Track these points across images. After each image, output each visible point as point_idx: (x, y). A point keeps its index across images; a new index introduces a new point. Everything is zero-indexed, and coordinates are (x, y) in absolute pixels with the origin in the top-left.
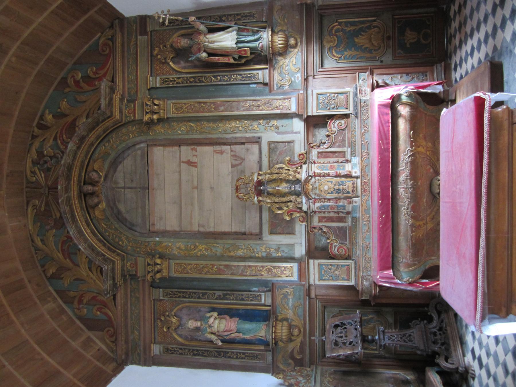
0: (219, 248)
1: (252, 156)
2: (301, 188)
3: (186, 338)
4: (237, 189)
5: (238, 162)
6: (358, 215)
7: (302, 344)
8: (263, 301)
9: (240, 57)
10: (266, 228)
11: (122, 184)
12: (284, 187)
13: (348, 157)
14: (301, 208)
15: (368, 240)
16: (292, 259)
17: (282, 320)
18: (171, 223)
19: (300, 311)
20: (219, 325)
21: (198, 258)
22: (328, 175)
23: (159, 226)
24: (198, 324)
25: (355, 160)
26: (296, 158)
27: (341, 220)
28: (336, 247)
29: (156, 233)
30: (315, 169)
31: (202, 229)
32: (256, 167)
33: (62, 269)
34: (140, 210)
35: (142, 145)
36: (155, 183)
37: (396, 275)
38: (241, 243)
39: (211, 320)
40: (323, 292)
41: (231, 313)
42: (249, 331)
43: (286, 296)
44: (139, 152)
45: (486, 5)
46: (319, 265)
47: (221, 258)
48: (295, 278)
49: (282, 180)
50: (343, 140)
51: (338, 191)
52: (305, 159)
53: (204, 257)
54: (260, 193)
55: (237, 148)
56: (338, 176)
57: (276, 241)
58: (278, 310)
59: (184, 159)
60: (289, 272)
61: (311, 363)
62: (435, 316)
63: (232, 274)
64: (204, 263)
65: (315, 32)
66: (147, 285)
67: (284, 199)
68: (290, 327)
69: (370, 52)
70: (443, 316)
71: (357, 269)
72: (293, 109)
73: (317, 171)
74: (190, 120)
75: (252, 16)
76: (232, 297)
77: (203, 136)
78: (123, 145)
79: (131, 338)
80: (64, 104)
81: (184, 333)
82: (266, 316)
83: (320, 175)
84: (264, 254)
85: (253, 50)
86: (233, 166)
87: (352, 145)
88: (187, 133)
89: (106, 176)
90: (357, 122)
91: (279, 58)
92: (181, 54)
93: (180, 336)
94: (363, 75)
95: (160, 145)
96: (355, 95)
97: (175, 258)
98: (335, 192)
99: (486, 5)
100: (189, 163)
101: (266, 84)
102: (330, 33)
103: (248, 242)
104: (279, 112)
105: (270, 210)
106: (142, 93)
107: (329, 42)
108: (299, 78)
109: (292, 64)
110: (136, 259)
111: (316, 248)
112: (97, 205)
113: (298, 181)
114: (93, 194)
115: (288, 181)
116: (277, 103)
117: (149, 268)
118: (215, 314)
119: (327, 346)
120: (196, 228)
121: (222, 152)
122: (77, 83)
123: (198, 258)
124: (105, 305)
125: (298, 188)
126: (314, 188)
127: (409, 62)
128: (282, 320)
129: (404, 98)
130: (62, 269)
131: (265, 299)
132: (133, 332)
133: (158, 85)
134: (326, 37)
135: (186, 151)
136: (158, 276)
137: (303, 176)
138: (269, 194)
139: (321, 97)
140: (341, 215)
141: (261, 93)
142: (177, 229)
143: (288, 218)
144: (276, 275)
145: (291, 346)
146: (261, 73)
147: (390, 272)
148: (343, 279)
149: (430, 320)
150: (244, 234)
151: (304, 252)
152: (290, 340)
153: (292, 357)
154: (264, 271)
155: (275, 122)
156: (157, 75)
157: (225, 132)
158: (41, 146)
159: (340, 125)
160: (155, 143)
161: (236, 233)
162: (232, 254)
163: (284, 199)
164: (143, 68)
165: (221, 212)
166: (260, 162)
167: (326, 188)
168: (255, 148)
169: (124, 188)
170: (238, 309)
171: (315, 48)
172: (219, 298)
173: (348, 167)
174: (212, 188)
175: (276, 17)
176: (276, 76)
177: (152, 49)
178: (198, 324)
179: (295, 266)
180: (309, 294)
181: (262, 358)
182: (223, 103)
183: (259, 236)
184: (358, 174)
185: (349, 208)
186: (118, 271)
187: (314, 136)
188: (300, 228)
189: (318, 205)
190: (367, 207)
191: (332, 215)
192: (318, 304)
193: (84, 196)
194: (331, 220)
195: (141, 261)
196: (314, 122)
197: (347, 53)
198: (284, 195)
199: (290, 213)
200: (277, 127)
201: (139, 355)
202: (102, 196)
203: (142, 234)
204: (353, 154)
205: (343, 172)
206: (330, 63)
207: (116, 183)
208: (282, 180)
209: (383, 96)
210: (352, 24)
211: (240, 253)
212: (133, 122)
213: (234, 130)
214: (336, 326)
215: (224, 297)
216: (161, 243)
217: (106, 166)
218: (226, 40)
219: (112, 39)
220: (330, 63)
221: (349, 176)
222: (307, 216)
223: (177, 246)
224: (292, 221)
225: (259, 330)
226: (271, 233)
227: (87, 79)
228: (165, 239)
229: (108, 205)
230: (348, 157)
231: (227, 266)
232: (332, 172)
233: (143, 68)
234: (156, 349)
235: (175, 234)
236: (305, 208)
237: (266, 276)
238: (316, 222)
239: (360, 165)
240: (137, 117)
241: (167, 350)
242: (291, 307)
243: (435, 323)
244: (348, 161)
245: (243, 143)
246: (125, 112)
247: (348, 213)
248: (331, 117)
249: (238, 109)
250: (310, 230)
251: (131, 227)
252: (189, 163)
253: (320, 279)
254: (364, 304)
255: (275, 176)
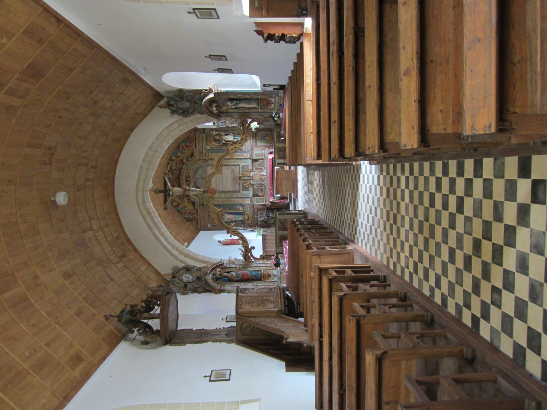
0: (228, 195)
2: (251, 178)
5: (233, 171)
7: (252, 221)
12: (246, 178)
15: (268, 192)
16: (249, 198)
21: (222, 198)
25: (265, 171)
27: (262, 186)
28: (260, 194)
30: (255, 173)
32: (238, 173)
33: (179, 204)
38: (234, 194)
40: (257, 206)
41: (232, 214)
45: (457, 304)
47: (229, 198)
48: (250, 202)
52: (252, 170)
54: (240, 180)
60: (248, 201)
68: (248, 216)
72: (249, 157)
76: (231, 208)
80: (179, 154)
82: (241, 214)
87: (264, 167)
92: (218, 141)
99: (457, 304)
105: (243, 184)
106: (204, 152)
108: (250, 148)
113: (250, 176)
114: (189, 181)
120: (221, 190)
122: (183, 147)
123: (222, 198)
124: (193, 213)
130: (179, 204)
145: (249, 222)
152: (248, 220)
154: (241, 201)
155: (244, 160)
158: (172, 165)
160: (208, 165)
165: (228, 185)
168: (238, 167)
171: (254, 140)
173: (263, 173)
183: (239, 191)
188: (251, 189)
190: (267, 183)
192: (256, 210)
193: (187, 181)
196: (254, 161)
199: (248, 185)
206: (258, 144)
211: (234, 196)
215: (230, 209)
218: (230, 138)
219: (195, 135)
220: (258, 144)
222: (253, 186)
224: (248, 187)
225: (240, 218)
226: (243, 190)
227: (186, 146)
234: (209, 226)
237: (241, 202)
238: (255, 187)
239: (265, 173)
241: (213, 226)
242: (248, 211)
250: (253, 190)
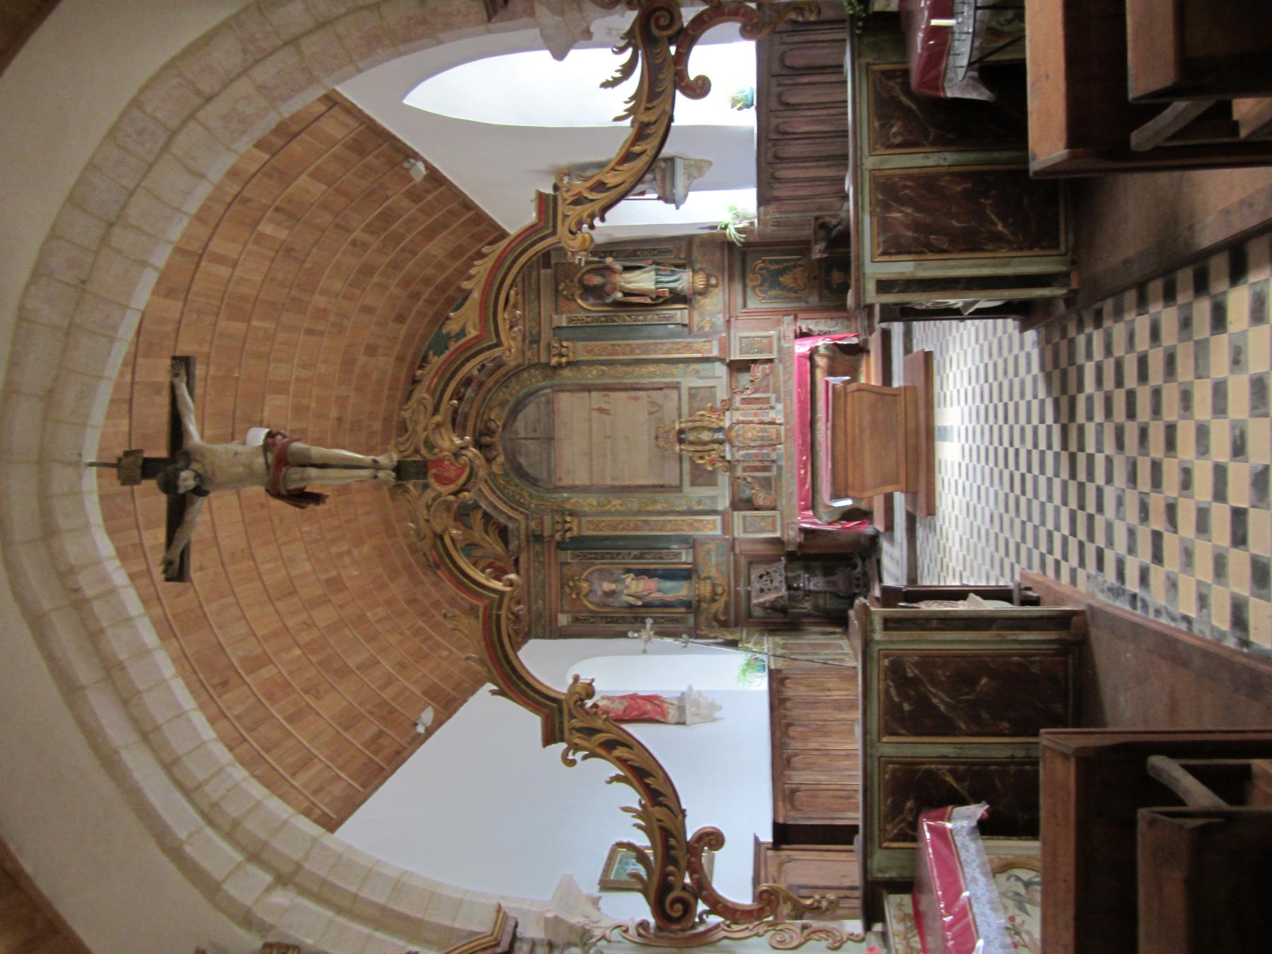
0: (634, 503)
1: (670, 402)
3: (598, 605)
4: (657, 438)
6: (782, 463)
7: (727, 604)
8: (684, 559)
9: (658, 297)
10: (687, 479)
11: (522, 434)
12: (706, 436)
13: (773, 403)
14: (723, 457)
15: (790, 488)
16: (715, 512)
17: (705, 579)
18: (581, 479)
19: (724, 568)
20: (635, 588)
21: (610, 513)
22: (752, 422)
23: (566, 482)
24: (613, 586)
25: (780, 407)
26: (719, 405)
27: (766, 469)
29: (564, 489)
30: (738, 416)
31: (616, 483)
34: (545, 463)
35: (547, 391)
36: (560, 433)
37: (815, 515)
38: (659, 497)
39: (628, 581)
40: (746, 547)
42: (670, 590)
43: (708, 553)
44: (543, 399)
46: (744, 517)
47: (639, 513)
49: (703, 428)
50: (768, 386)
51: (762, 438)
52: (728, 406)
53: (619, 513)
54: (681, 441)
55: (653, 393)
56: (762, 423)
57: (696, 494)
58: (700, 568)
59: (595, 406)
60: (712, 528)
61: (736, 625)
62: (860, 564)
63: (651, 530)
64: (619, 519)
65: (737, 272)
66: (553, 545)
67: (708, 448)
68: (714, 586)
69: (796, 292)
70: (867, 562)
71: (782, 519)
73: (741, 418)
74: (602, 363)
75: (670, 251)
77: (617, 381)
78: (525, 391)
79: (534, 608)
81: (595, 599)
82: (686, 575)
83: (743, 422)
84: (685, 508)
85: (672, 291)
86: (650, 413)
87: (776, 390)
88: (599, 377)
89: (504, 426)
90: (781, 366)
91: (699, 298)
93: (591, 603)
94: (788, 319)
95: (568, 391)
96: (779, 340)
97: (586, 514)
98: (878, 927)
100: (601, 410)
101: (685, 325)
102: (754, 272)
103: (666, 495)
104: (699, 355)
105: (692, 461)
106: (546, 335)
107: (752, 280)
108: (720, 320)
109: (713, 306)
110: (542, 518)
111: (740, 500)
112: (495, 458)
113: (721, 429)
115: (710, 429)
116: (697, 346)
117: (558, 527)
118: (632, 575)
119: (753, 594)
120: (609, 482)
121: (637, 399)
123: (610, 513)
125: (720, 436)
126: (738, 436)
127: (833, 304)
128: (705, 579)
129: (822, 350)
131: (686, 557)
132: (536, 601)
133: (564, 324)
134: (750, 276)
135: (597, 398)
136: (568, 535)
137: (727, 424)
138: (691, 443)
139: (745, 341)
140: (767, 464)
141: (679, 335)
142: (587, 483)
143: (710, 468)
144: (698, 529)
145: (715, 607)
146: (679, 313)
147: (811, 513)
148: (769, 531)
149: (855, 567)
150: (662, 486)
151: (727, 504)
152: (713, 600)
153: (716, 619)
154: (684, 526)
156: (562, 313)
157: (642, 376)
159: (764, 369)
160: (561, 389)
161: (654, 486)
162: (650, 508)
163: (708, 448)
164: (546, 304)
166: (679, 409)
167: (750, 435)
168: (674, 394)
169: (526, 439)
170: (656, 570)
171: (738, 287)
172: (635, 557)
174: (626, 438)
175: (696, 254)
176: (696, 318)
177: (557, 284)
178: (613, 586)
179: (718, 518)
180: (733, 549)
181: (684, 620)
182: (639, 346)
183: (679, 488)
184: (782, 421)
185: (774, 456)
186: (523, 532)
187: (737, 381)
188: (724, 478)
189: (742, 452)
190: (788, 454)
191: (757, 464)
192: (743, 561)
194: (756, 469)
195: (547, 519)
196: (738, 367)
197: (773, 293)
198: (706, 443)
199: (712, 463)
200: (698, 372)
201: (544, 627)
202: (500, 448)
203: (548, 491)
204: (778, 400)
205: (767, 419)
206: (753, 304)
207: (516, 433)
208: (703, 428)
209: (802, 347)
210: (777, 262)
211: (658, 507)
212: (538, 365)
213: (651, 375)
214: (761, 577)
215: (641, 556)
216: (569, 499)
217: (505, 415)
218: (644, 281)
221: (772, 423)
222: (731, 466)
223: (588, 502)
224: (714, 472)
225: (679, 591)
226: (693, 484)
228: (574, 495)
229: (507, 458)
230: (773, 403)
231: (645, 521)
232: (755, 419)
233: (546, 304)
234: (563, 620)
235: (586, 490)
236: (728, 457)
237: (688, 532)
238: (739, 472)
240: (543, 359)
241: (576, 620)
242: (714, 567)
243: (859, 569)
244: (772, 408)
245: (661, 389)
246: (528, 354)
247: (773, 461)
248: (754, 361)
249: (655, 352)
250: (734, 481)
251: (534, 482)
252: (601, 410)
253: (745, 531)
254: (791, 557)
255: (698, 424)
